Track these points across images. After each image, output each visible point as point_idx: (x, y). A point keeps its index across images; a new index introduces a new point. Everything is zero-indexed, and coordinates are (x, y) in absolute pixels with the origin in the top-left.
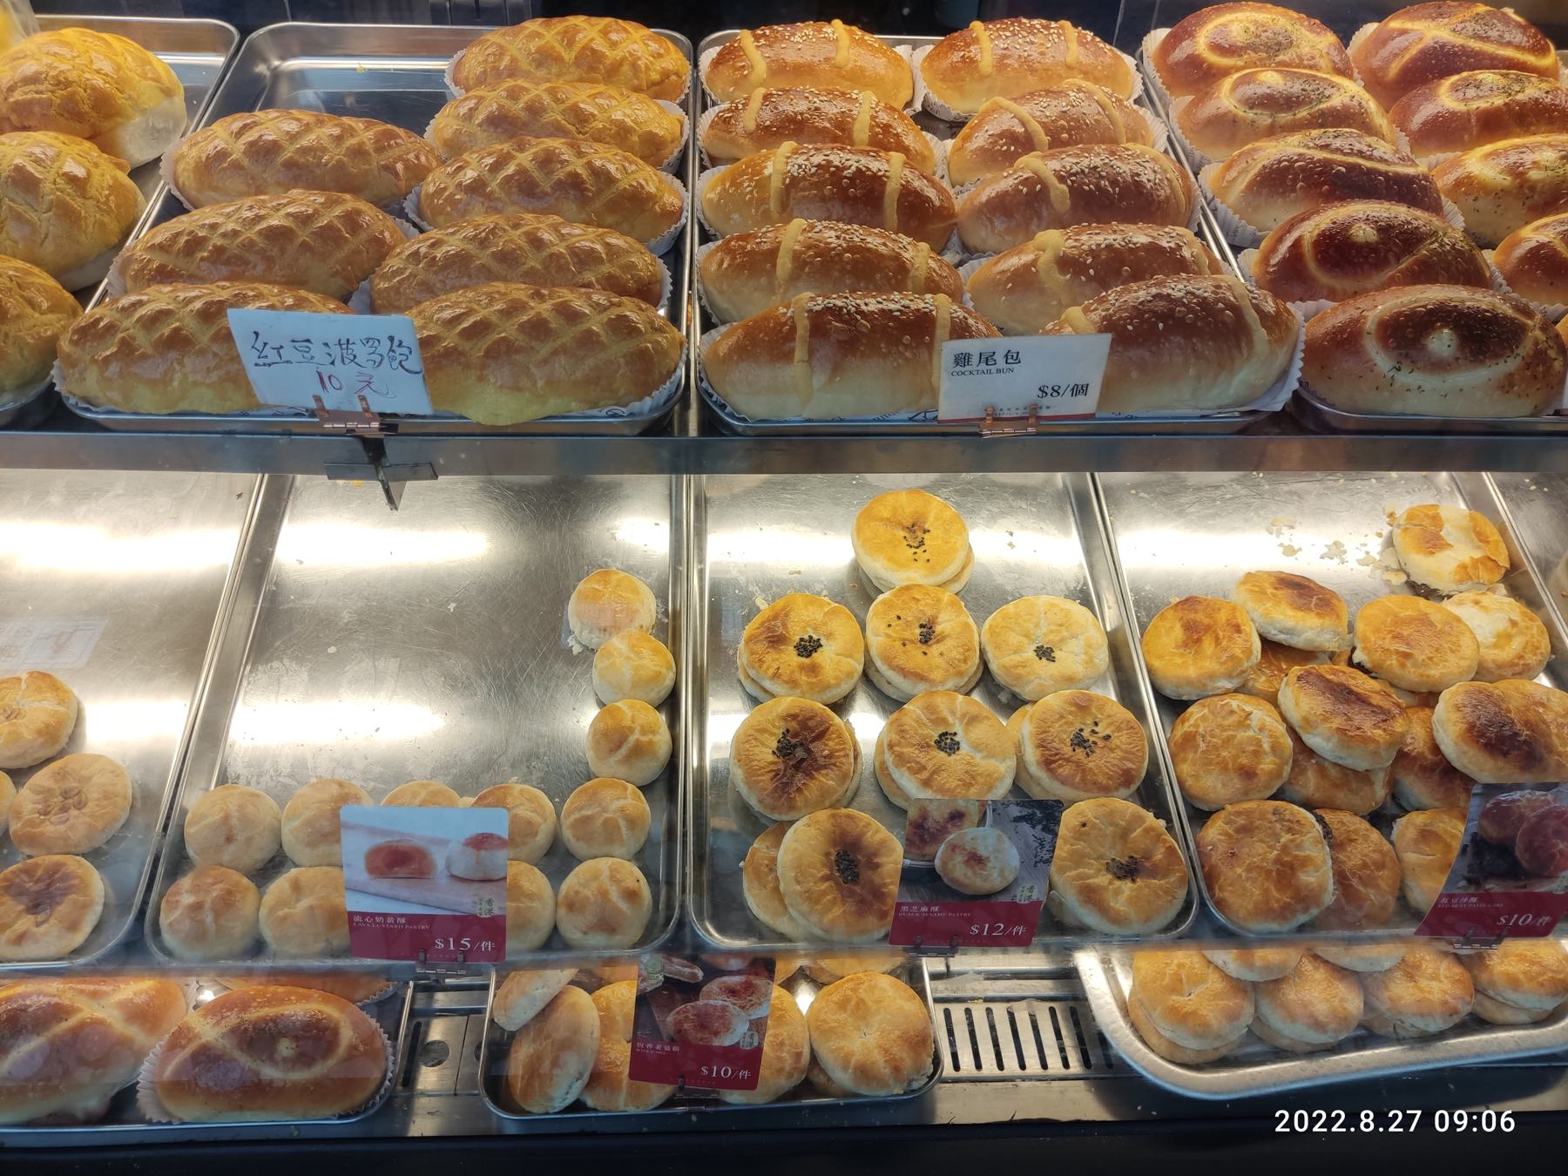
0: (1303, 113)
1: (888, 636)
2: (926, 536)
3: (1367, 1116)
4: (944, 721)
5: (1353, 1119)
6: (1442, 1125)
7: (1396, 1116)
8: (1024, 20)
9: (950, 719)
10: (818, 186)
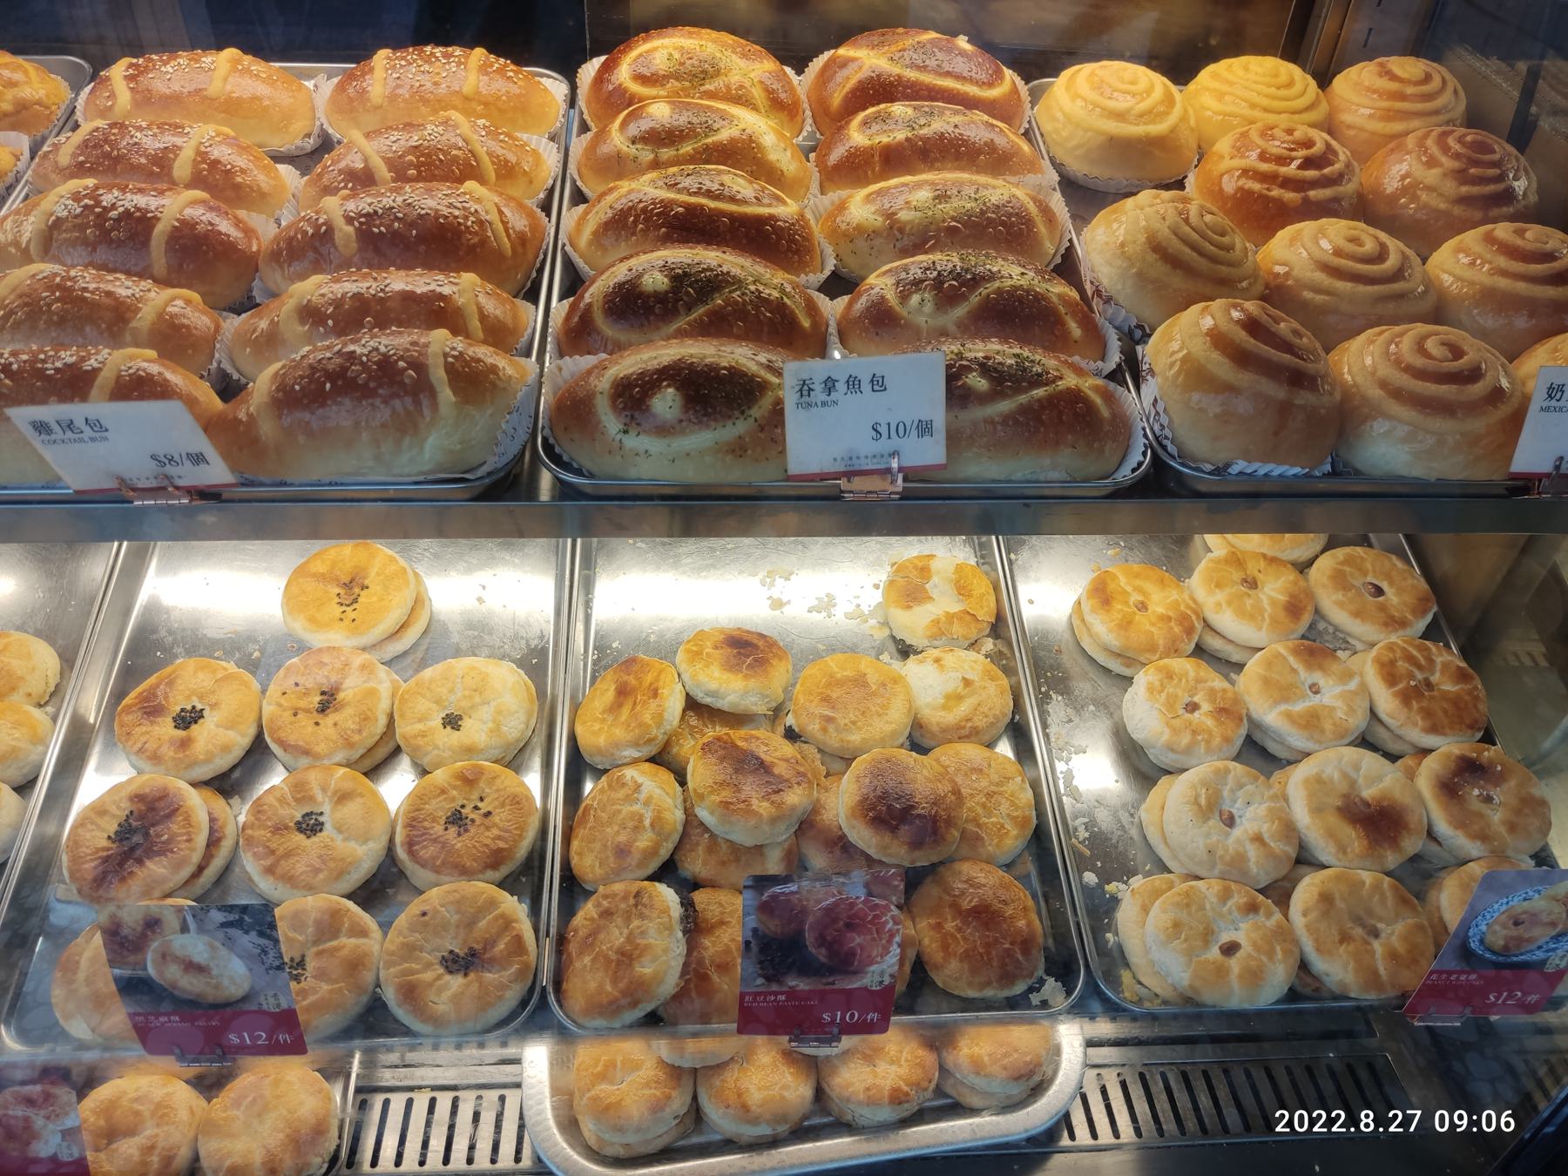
0: (687, 148)
1: (280, 705)
2: (365, 592)
3: (1367, 1116)
4: (312, 799)
5: (1353, 1120)
6: (1442, 1126)
7: (1396, 1116)
8: (155, 57)
9: (319, 796)
10: (82, 228)
